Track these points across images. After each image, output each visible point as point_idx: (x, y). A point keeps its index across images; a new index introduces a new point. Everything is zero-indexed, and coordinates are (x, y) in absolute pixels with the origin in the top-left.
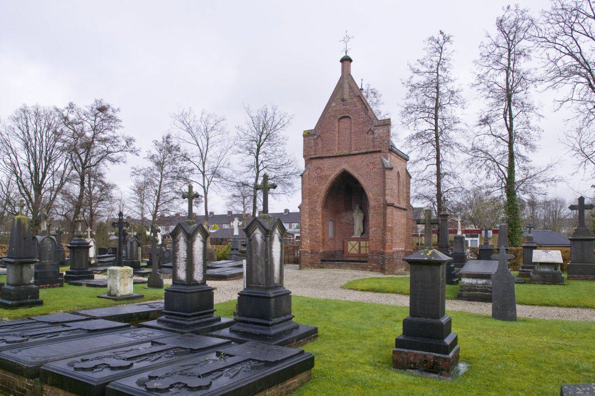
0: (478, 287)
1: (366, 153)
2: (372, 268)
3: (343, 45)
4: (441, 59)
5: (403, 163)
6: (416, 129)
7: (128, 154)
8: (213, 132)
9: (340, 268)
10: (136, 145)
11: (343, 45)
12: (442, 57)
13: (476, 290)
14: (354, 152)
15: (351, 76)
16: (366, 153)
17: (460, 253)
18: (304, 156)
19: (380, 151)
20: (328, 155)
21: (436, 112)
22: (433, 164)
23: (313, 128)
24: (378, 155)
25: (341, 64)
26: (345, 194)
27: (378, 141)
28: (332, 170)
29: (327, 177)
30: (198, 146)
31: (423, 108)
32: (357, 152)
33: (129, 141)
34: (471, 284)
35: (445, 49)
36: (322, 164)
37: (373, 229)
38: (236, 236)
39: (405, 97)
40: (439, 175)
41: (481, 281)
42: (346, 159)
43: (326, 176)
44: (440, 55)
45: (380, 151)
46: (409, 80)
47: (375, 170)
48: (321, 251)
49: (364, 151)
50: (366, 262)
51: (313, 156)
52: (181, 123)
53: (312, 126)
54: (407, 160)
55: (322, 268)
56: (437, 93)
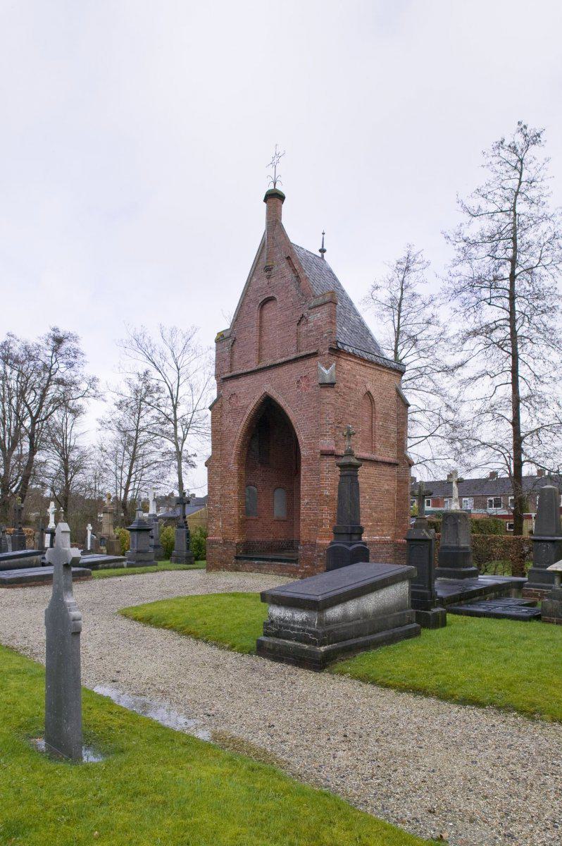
0: (293, 629)
1: (296, 360)
2: (304, 573)
3: (271, 171)
4: (520, 183)
5: (394, 379)
6: (477, 320)
7: (91, 400)
8: (186, 356)
9: (260, 570)
10: (101, 387)
11: (271, 171)
12: (523, 179)
13: (289, 637)
14: (279, 361)
15: (281, 226)
16: (296, 360)
17: (453, 548)
18: (217, 376)
19: (315, 354)
20: (245, 371)
21: (512, 285)
22: (507, 384)
23: (228, 327)
24: (311, 362)
25: (265, 204)
26: (265, 442)
27: (313, 336)
28: (249, 395)
29: (244, 407)
30: (166, 382)
31: (494, 283)
32: (283, 360)
33: (93, 381)
34: (282, 620)
35: (546, 169)
36: (238, 387)
37: (306, 501)
38: (515, 521)
39: (450, 263)
40: (516, 401)
41: (300, 616)
42: (268, 374)
43: (243, 407)
44: (518, 176)
45: (315, 354)
46: (457, 230)
47: (310, 390)
48: (237, 540)
49: (293, 356)
50: (296, 561)
51: (226, 375)
52: (169, 350)
53: (225, 325)
54: (402, 373)
55: (237, 570)
56: (515, 248)
